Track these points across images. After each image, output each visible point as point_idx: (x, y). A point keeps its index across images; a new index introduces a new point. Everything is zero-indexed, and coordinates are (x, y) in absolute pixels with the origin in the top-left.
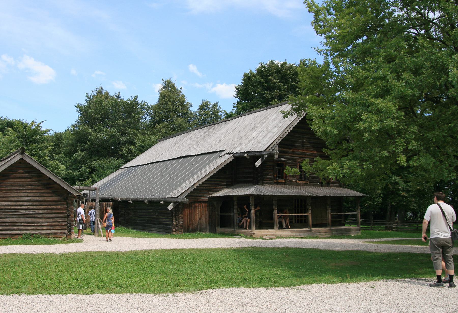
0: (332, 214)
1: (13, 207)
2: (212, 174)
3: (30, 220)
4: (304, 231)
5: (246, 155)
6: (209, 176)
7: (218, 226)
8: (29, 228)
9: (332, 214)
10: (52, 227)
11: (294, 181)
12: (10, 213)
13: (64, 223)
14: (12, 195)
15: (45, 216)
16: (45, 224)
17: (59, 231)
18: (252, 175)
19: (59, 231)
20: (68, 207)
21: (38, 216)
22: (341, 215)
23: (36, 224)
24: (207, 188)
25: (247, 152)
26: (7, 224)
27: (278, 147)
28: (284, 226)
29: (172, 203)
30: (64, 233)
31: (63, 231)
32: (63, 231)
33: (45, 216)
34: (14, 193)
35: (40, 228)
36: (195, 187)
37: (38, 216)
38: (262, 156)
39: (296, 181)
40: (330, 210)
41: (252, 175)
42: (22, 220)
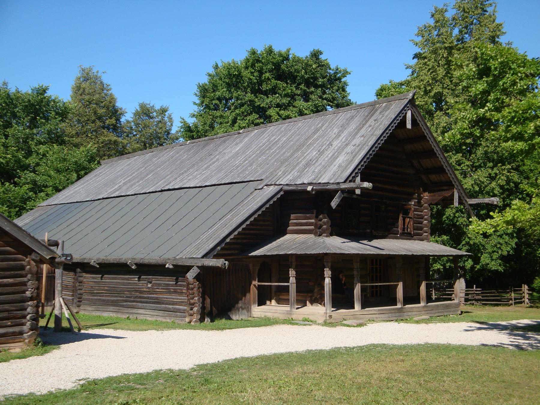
4: (390, 310)
5: (309, 188)
7: (254, 303)
18: (313, 221)
24: (239, 241)
25: (310, 184)
29: (195, 268)
36: (228, 240)
41: (313, 221)
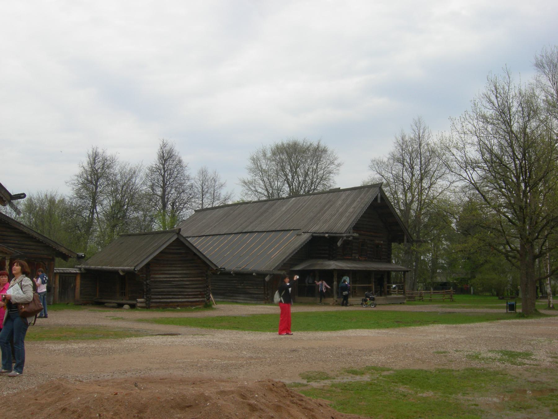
0: (388, 285)
1: (168, 279)
2: (296, 251)
3: (181, 290)
6: (295, 253)
8: (180, 297)
9: (388, 285)
10: (195, 296)
11: (357, 257)
12: (166, 284)
13: (203, 293)
14: (168, 268)
15: (191, 286)
16: (191, 294)
17: (201, 299)
19: (201, 299)
20: (207, 279)
21: (186, 286)
22: (356, 286)
23: (185, 294)
26: (164, 293)
27: (353, 230)
28: (51, 303)
29: (268, 275)
30: (204, 301)
31: (203, 299)
32: (203, 299)
33: (191, 286)
34: (169, 267)
35: (187, 297)
37: (186, 286)
38: (342, 237)
39: (359, 258)
40: (386, 282)
42: (175, 289)
